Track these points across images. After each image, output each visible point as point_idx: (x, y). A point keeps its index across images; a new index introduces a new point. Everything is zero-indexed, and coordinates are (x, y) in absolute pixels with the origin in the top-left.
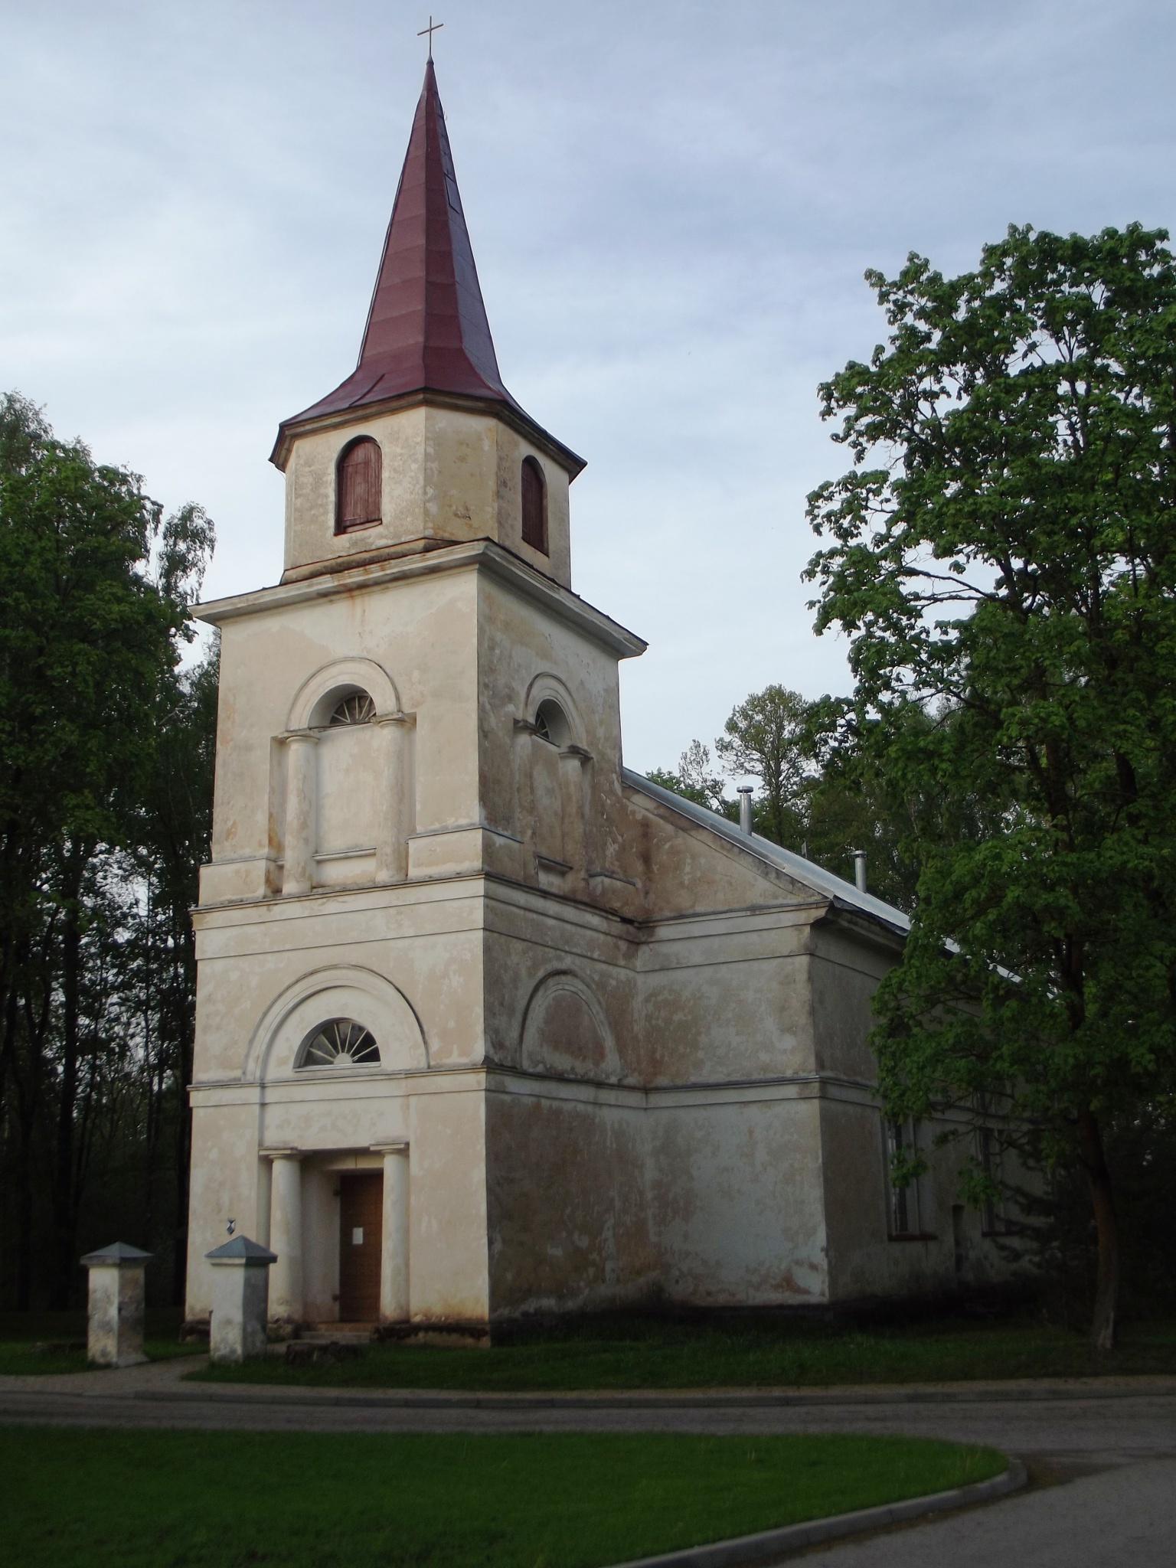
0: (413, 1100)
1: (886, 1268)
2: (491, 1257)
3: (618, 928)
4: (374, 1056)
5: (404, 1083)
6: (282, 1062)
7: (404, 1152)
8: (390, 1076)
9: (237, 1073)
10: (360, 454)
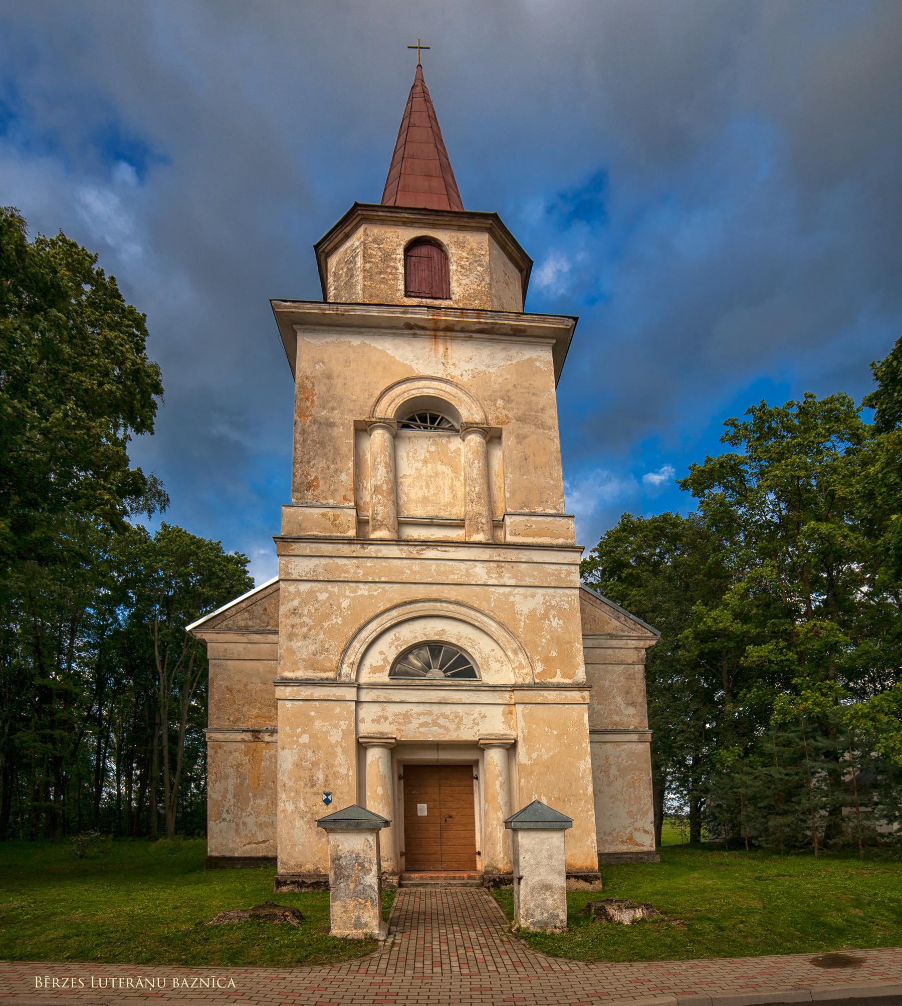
0: (519, 708)
4: (470, 673)
5: (507, 695)
6: (375, 670)
7: (511, 748)
9: (331, 675)
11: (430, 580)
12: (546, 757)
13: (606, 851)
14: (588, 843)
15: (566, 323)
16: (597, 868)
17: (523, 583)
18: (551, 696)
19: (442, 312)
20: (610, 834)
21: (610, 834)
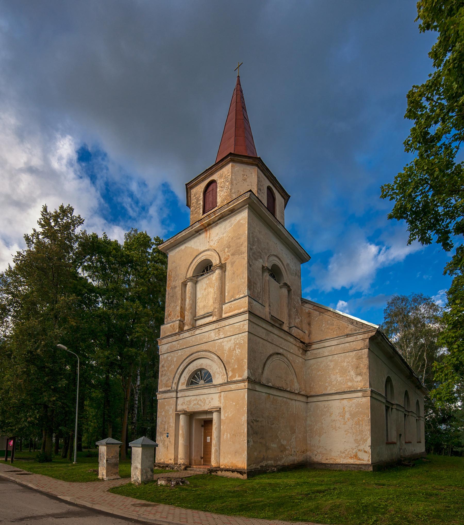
0: (222, 393)
1: (386, 454)
2: (248, 447)
3: (301, 345)
4: (211, 381)
8: (215, 386)
9: (170, 388)
10: (210, 188)
11: (197, 343)
12: (230, 416)
13: (341, 462)
14: (244, 456)
15: (247, 195)
16: (246, 468)
17: (227, 336)
18: (233, 386)
19: (203, 220)
20: (344, 452)
21: (344, 452)
